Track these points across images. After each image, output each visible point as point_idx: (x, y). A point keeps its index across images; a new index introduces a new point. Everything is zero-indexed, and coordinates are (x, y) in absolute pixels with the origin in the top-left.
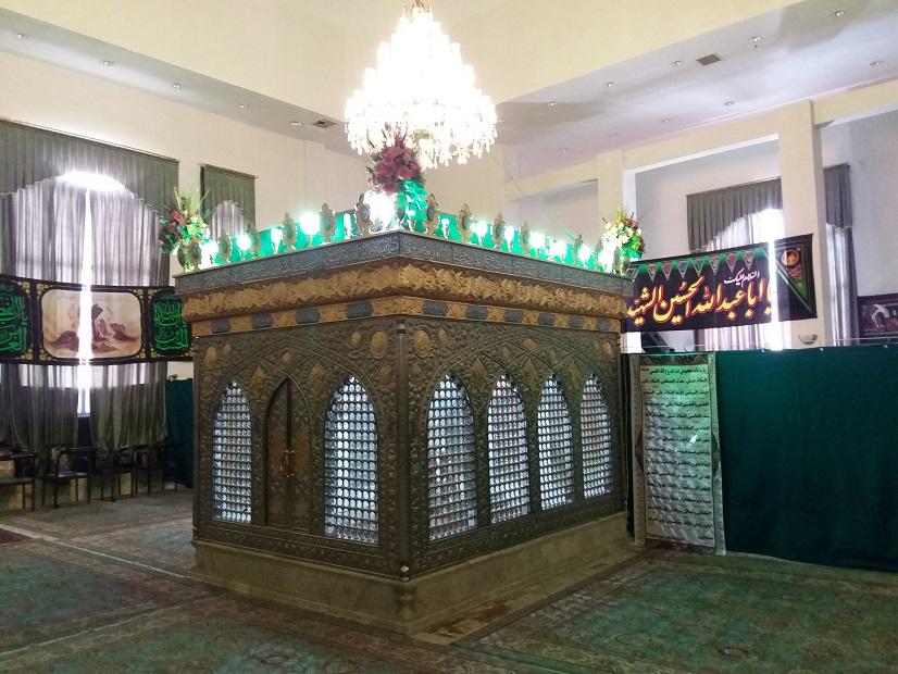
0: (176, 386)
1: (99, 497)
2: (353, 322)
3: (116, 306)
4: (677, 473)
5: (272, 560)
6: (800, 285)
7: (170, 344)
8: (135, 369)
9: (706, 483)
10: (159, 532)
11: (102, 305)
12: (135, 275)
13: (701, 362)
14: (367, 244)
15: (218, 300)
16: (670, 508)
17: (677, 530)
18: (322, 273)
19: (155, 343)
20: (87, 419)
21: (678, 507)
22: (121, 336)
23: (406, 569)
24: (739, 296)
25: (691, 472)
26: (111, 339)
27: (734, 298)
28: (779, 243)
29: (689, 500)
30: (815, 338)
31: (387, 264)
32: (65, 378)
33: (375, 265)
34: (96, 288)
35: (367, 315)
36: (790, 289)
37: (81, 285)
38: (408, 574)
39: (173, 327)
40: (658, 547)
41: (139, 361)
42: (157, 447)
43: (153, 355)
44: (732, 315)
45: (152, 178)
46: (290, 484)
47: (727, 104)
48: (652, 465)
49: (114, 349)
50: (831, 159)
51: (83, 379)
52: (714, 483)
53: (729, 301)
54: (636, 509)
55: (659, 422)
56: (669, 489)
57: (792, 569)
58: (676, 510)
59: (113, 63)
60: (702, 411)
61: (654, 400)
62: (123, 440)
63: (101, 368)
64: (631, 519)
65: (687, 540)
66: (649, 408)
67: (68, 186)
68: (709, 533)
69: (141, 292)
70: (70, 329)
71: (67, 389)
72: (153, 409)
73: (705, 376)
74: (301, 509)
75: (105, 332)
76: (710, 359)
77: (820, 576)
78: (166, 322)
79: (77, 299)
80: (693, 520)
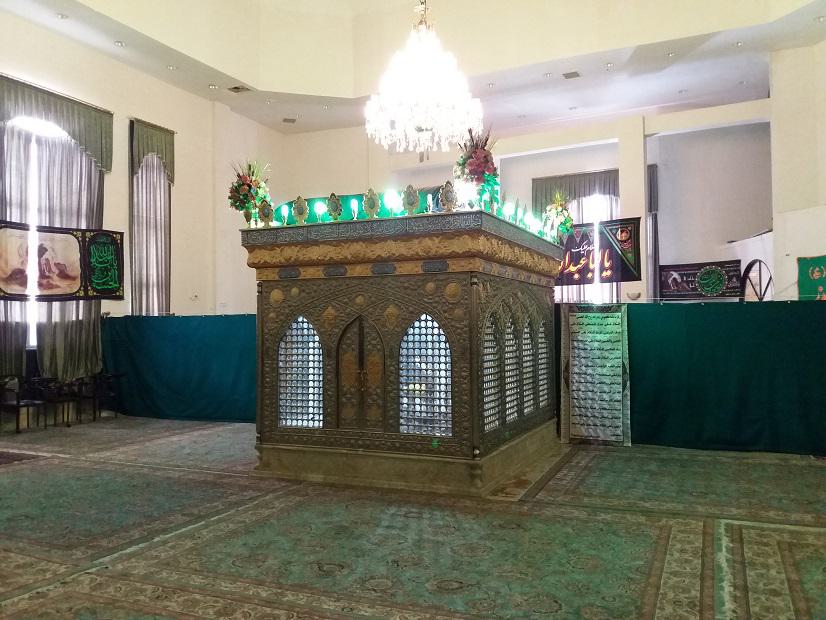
0: (109, 323)
1: (91, 417)
2: (429, 275)
3: (58, 246)
4: (595, 390)
5: (347, 454)
6: (630, 255)
7: (104, 284)
8: (74, 306)
9: (618, 397)
10: (229, 443)
11: (47, 245)
12: (75, 219)
13: (617, 311)
14: (451, 219)
15: (292, 253)
16: (589, 415)
17: (595, 431)
18: (406, 237)
19: (91, 282)
20: (34, 351)
21: (597, 415)
22: (64, 275)
23: (478, 452)
24: (582, 262)
25: (606, 388)
26: (55, 277)
27: (579, 263)
28: (602, 223)
29: (605, 409)
30: (639, 296)
31: (469, 235)
32: (15, 312)
33: (459, 233)
34: (41, 229)
35: (443, 270)
36: (623, 260)
37: (38, 231)
38: (481, 455)
39: (106, 267)
40: (580, 443)
41: (78, 299)
42: (94, 377)
43: (91, 293)
44: (576, 276)
45: (90, 127)
46: (363, 396)
47: (571, 109)
48: (576, 384)
49: (58, 287)
50: (650, 162)
51: (31, 314)
52: (624, 396)
53: (575, 265)
54: (562, 417)
55: (583, 354)
56: (590, 402)
57: (685, 453)
58: (594, 416)
59: (67, 17)
60: (615, 345)
61: (580, 338)
62: (65, 371)
63: (44, 304)
64: (558, 424)
65: (602, 437)
66: (576, 344)
67: (16, 130)
68: (619, 432)
69: (79, 234)
70: (19, 266)
71: (17, 323)
72: (90, 346)
73: (619, 321)
74: (374, 414)
75: (50, 271)
76: (623, 309)
77: (703, 455)
78: (100, 263)
79: (24, 238)
80: (607, 423)
